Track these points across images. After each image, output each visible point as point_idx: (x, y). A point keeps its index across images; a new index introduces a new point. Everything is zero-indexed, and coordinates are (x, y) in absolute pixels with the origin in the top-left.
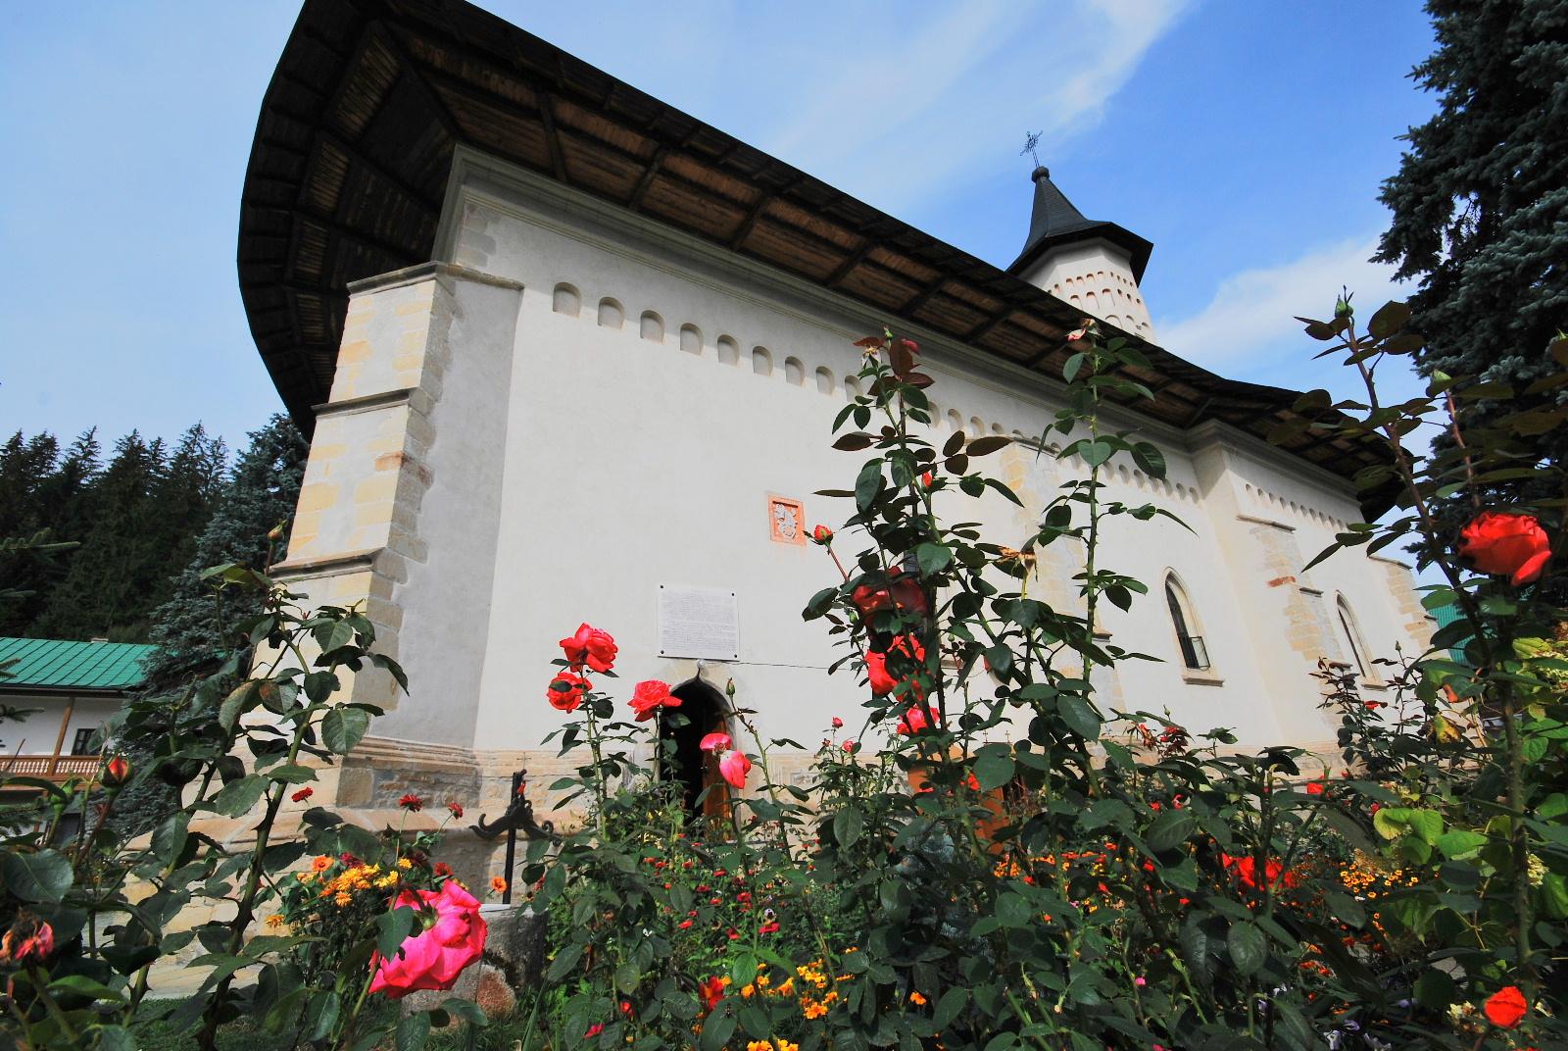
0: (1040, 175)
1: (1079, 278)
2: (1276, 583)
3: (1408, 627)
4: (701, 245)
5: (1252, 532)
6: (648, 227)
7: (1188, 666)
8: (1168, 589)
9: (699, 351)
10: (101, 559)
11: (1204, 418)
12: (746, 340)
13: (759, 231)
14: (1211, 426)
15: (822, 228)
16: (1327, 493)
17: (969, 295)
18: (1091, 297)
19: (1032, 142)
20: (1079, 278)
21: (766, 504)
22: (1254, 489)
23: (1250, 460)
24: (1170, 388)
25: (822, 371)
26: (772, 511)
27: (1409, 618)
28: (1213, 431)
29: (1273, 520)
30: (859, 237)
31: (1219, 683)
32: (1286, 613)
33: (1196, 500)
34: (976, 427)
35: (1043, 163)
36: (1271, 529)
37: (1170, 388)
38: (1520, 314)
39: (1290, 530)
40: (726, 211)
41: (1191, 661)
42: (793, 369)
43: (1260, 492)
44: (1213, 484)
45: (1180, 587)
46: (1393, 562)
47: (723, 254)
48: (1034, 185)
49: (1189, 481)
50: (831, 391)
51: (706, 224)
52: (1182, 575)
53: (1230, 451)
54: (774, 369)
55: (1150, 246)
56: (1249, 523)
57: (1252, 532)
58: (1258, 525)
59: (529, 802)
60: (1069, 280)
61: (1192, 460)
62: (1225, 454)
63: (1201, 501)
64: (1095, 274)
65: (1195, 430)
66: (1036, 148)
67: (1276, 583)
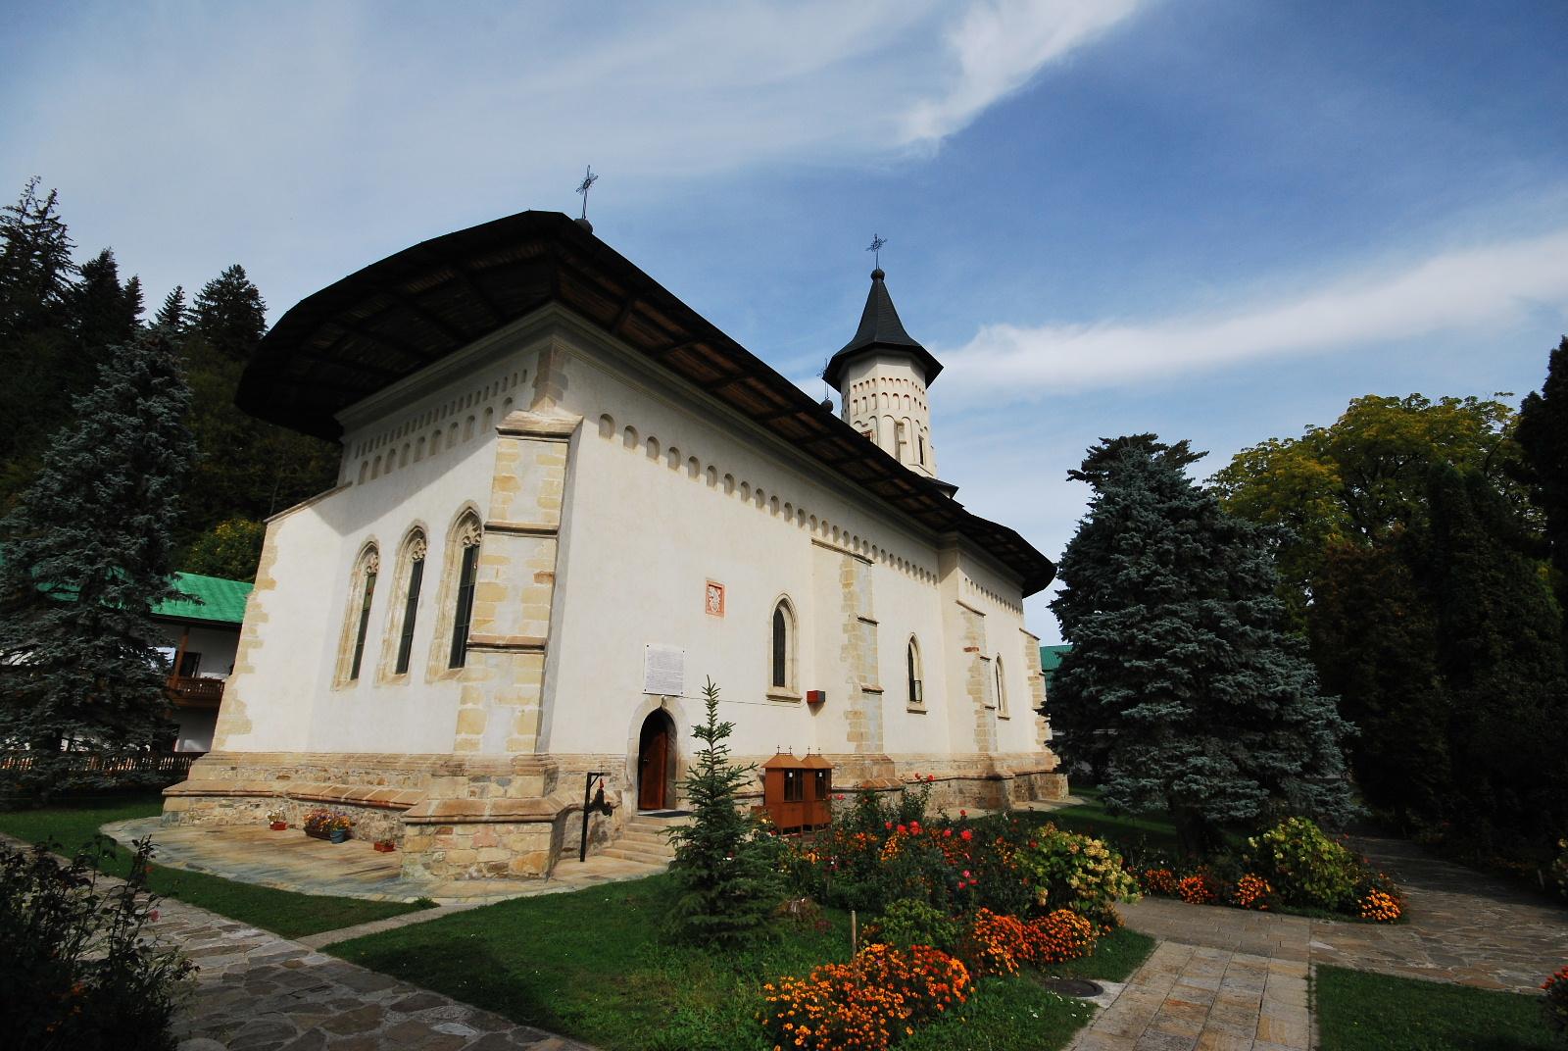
0: (878, 276)
1: (895, 395)
2: (968, 650)
3: (1029, 679)
4: (688, 386)
5: (963, 613)
6: (658, 371)
9: (656, 457)
11: (953, 530)
12: (621, 421)
13: (680, 353)
14: (954, 535)
15: (769, 393)
17: (844, 445)
18: (896, 397)
19: (877, 244)
20: (895, 395)
21: (704, 586)
22: (969, 581)
23: (971, 560)
25: (693, 460)
27: (1031, 673)
28: (956, 539)
31: (924, 713)
32: (970, 671)
33: (935, 583)
36: (973, 615)
39: (983, 615)
41: (913, 698)
42: (606, 423)
43: (972, 583)
44: (947, 575)
46: (1031, 635)
47: (700, 393)
48: (871, 282)
49: (934, 571)
51: (695, 373)
52: (920, 640)
54: (660, 456)
57: (963, 613)
58: (965, 609)
59: (1351, 403)
60: (883, 379)
61: (939, 555)
62: (959, 555)
63: (938, 584)
64: (902, 380)
65: (947, 535)
67: (968, 650)
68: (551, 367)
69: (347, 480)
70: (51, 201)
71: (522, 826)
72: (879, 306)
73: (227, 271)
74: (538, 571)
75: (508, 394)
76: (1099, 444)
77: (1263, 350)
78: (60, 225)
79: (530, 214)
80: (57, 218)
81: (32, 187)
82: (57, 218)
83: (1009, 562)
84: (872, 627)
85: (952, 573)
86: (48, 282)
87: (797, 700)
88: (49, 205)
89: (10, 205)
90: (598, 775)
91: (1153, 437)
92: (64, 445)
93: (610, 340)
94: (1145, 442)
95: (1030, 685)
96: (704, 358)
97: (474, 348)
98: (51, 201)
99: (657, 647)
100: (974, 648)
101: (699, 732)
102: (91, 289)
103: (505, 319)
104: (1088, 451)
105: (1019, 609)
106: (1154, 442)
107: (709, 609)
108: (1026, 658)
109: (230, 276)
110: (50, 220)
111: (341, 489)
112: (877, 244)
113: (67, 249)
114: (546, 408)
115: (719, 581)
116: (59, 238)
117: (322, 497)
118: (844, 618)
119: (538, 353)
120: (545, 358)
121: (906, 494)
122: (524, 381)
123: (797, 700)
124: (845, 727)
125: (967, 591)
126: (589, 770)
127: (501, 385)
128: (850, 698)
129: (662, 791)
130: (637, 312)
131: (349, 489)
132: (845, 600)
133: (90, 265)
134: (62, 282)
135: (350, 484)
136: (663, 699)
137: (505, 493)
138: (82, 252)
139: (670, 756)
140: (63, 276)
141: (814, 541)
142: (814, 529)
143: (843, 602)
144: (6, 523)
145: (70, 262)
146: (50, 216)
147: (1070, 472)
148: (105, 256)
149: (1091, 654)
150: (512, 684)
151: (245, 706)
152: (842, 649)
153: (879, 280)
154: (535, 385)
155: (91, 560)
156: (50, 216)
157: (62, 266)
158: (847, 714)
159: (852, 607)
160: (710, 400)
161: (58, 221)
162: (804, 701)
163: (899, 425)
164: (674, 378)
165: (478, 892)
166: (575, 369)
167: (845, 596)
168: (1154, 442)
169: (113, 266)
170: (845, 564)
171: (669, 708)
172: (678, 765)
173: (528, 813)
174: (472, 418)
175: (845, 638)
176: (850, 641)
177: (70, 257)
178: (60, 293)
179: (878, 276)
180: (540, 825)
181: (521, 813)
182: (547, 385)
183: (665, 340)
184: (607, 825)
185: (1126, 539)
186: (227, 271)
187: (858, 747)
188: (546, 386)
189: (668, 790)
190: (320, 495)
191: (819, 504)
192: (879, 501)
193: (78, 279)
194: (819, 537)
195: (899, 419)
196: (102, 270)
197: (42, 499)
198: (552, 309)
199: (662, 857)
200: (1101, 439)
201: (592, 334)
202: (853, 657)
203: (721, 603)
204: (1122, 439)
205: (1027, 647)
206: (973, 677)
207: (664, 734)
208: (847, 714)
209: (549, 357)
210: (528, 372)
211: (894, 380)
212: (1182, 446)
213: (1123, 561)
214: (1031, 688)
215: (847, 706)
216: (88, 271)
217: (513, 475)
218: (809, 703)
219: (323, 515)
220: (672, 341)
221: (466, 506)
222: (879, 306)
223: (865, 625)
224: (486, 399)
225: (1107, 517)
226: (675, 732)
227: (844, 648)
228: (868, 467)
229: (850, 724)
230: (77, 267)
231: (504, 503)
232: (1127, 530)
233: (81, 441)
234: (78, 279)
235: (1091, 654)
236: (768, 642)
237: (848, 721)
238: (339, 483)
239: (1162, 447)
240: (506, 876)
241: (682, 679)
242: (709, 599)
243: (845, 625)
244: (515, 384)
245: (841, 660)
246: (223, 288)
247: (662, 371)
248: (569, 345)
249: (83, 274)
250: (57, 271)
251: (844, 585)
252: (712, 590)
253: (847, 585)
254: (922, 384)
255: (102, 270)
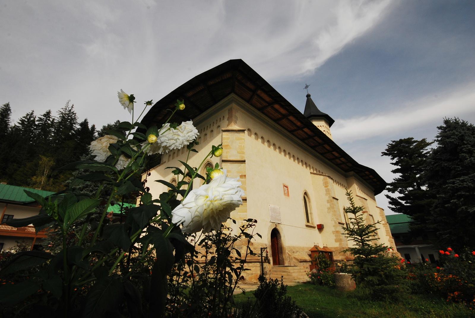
0: (308, 96)
5: (359, 199)
7: (307, 222)
8: (304, 197)
10: (46, 162)
11: (351, 171)
13: (269, 109)
14: (352, 173)
16: (361, 184)
19: (307, 87)
21: (282, 186)
24: (347, 164)
26: (284, 187)
29: (382, 208)
30: (287, 112)
34: (256, 136)
35: (309, 93)
36: (364, 200)
37: (347, 164)
38: (451, 202)
40: (279, 115)
45: (307, 197)
48: (306, 98)
49: (346, 186)
50: (257, 139)
53: (355, 179)
54: (259, 139)
55: (334, 121)
56: (359, 197)
57: (359, 199)
58: (360, 198)
61: (346, 180)
62: (354, 179)
66: (308, 89)
68: (233, 113)
69: (164, 161)
70: (72, 107)
71: (249, 264)
73: (116, 122)
74: (241, 175)
75: (218, 124)
76: (391, 143)
77: (422, 118)
78: (74, 113)
79: (231, 60)
80: (74, 112)
81: (68, 103)
82: (74, 112)
83: (373, 183)
84: (336, 201)
85: (353, 185)
86: (71, 128)
87: (314, 227)
88: (72, 108)
89: (62, 108)
90: (265, 248)
91: (412, 138)
92: (85, 159)
93: (248, 105)
94: (409, 141)
95: (384, 227)
96: (277, 111)
97: (205, 114)
98: (72, 107)
99: (272, 206)
100: (366, 212)
101: (346, 211)
102: (82, 129)
103: (216, 102)
104: (388, 146)
105: (374, 200)
106: (413, 140)
107: (285, 194)
108: (381, 217)
109: (117, 123)
110: (72, 112)
111: (162, 164)
112: (307, 87)
113: (76, 119)
114: (233, 126)
115: (287, 184)
116: (74, 116)
117: (158, 167)
118: (327, 198)
119: (228, 110)
120: (230, 111)
121: (337, 158)
122: (223, 119)
123: (314, 227)
124: (333, 237)
125: (359, 192)
126: (261, 247)
127: (209, 127)
128: (334, 226)
129: (278, 259)
130: (258, 96)
131: (165, 164)
132: (326, 192)
133: (82, 123)
134: (75, 128)
135: (165, 162)
136: (276, 224)
137: (227, 150)
138: (80, 120)
139: (279, 246)
140: (75, 126)
141: (311, 173)
142: (310, 169)
143: (325, 193)
144: (68, 182)
145: (77, 122)
146: (72, 111)
147: (382, 153)
148: (86, 120)
149: (460, 193)
150: (237, 213)
151: (212, 179)
152: (328, 209)
153: (309, 97)
154: (228, 120)
155: (91, 191)
156: (72, 111)
157: (75, 124)
158: (333, 232)
159: (329, 194)
160: (277, 125)
161: (74, 112)
162: (316, 228)
164: (266, 118)
165: (342, 251)
166: (239, 114)
167: (326, 190)
168: (413, 140)
169: (87, 123)
171: (278, 228)
172: (283, 248)
173: (251, 259)
174: (206, 135)
175: (328, 205)
176: (330, 206)
177: (77, 121)
178: (74, 131)
179: (308, 96)
180: (256, 264)
181: (249, 259)
182: (232, 119)
183: (265, 104)
184: (267, 269)
185: (465, 148)
186: (116, 122)
187: (340, 244)
188: (230, 120)
189: (280, 258)
190: (157, 166)
191: (310, 161)
192: (327, 161)
193: (79, 127)
194: (312, 171)
196: (84, 124)
197: (78, 174)
198: (233, 95)
199: (293, 280)
200: (392, 141)
201: (243, 103)
202: (333, 211)
203: (288, 191)
204: (401, 140)
205: (380, 213)
206: (367, 222)
207: (276, 238)
208: (333, 232)
209: (232, 110)
210: (225, 117)
212: (423, 141)
213: (466, 156)
214: (384, 228)
215: (333, 229)
216: (81, 124)
217: (229, 144)
218: (318, 229)
219: (158, 172)
220: (267, 104)
221: (207, 161)
223: (335, 200)
224: (210, 127)
225: (454, 140)
226: (280, 237)
227: (329, 209)
228: (325, 148)
229: (335, 236)
230: (79, 124)
231: (226, 153)
232: (464, 144)
233: (89, 157)
234: (79, 127)
235: (460, 193)
236: (303, 206)
237: (335, 235)
238: (161, 163)
239: (415, 142)
240: (246, 283)
241: (280, 217)
242: (284, 190)
243: (328, 200)
244: (220, 121)
245: (328, 213)
246: (115, 126)
247: (263, 116)
248: (237, 107)
249: (80, 125)
250: (74, 125)
251: (325, 186)
252: (285, 187)
253: (326, 187)
254: (328, 127)
255: (84, 124)
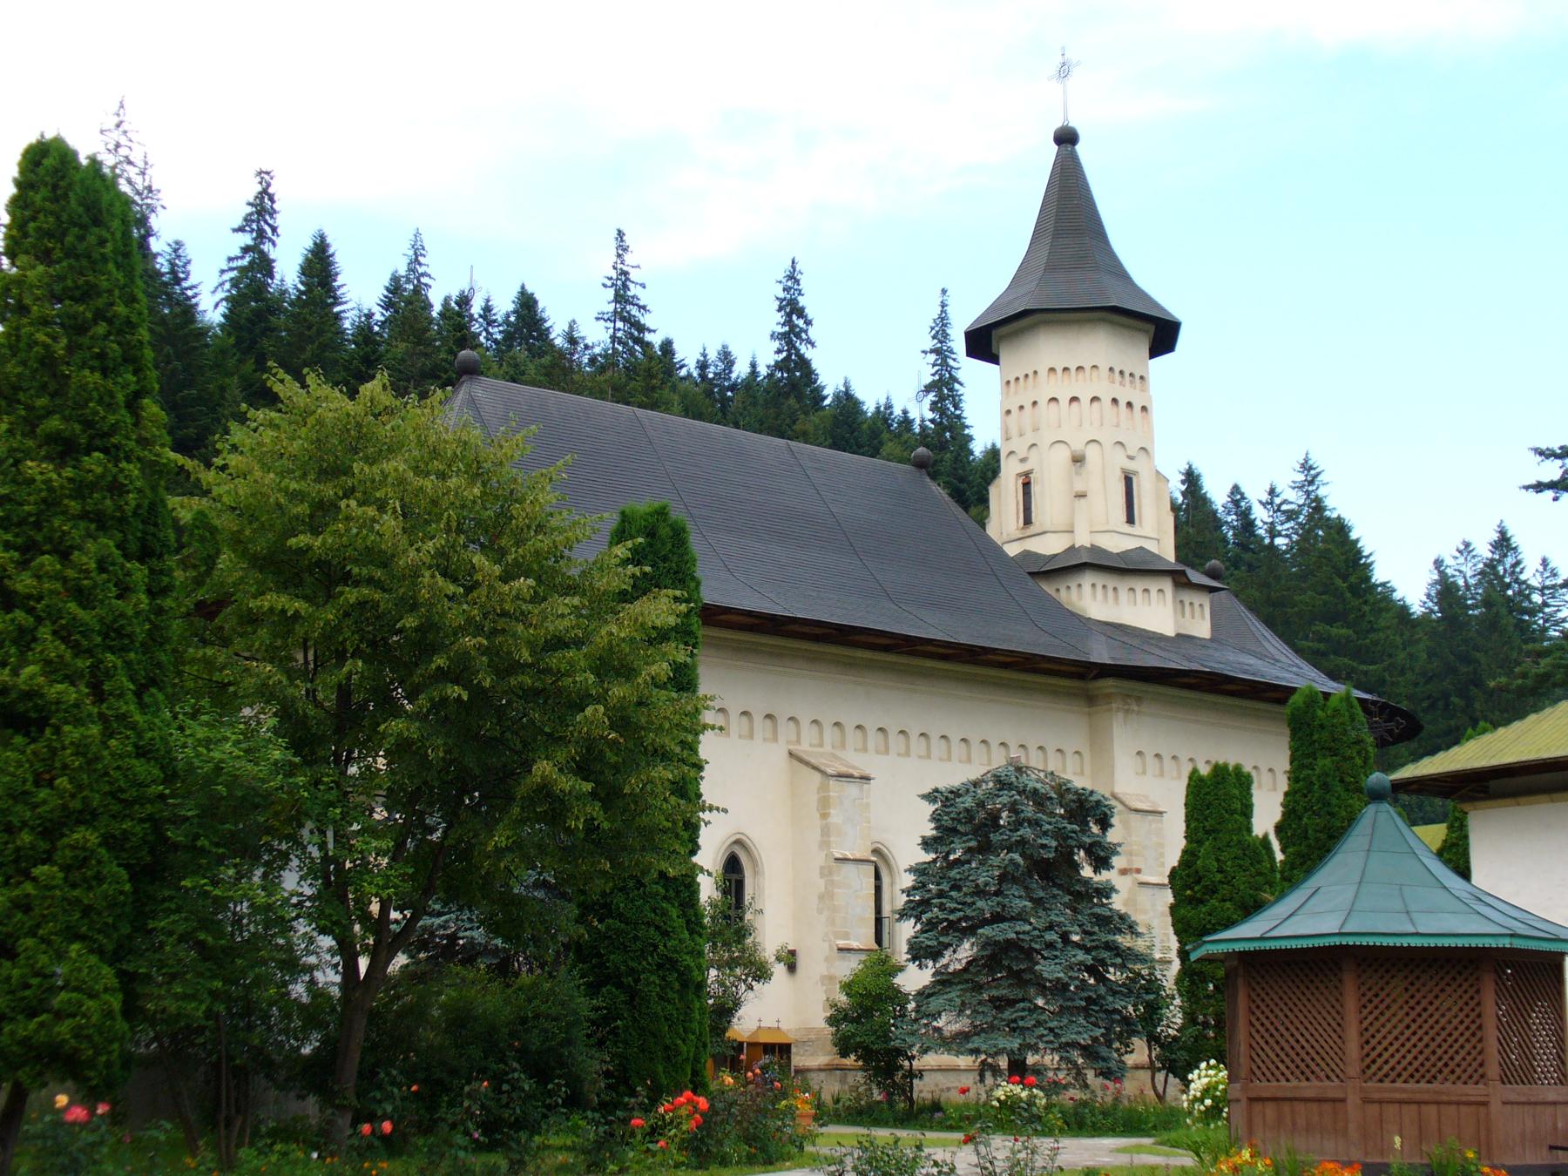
0: (1066, 138)
72: (1069, 213)
158: (823, 978)
163: (1078, 460)
170: (823, 788)
179: (1066, 138)
195: (1078, 446)
211: (1059, 371)
222: (1069, 213)
253: (824, 816)
